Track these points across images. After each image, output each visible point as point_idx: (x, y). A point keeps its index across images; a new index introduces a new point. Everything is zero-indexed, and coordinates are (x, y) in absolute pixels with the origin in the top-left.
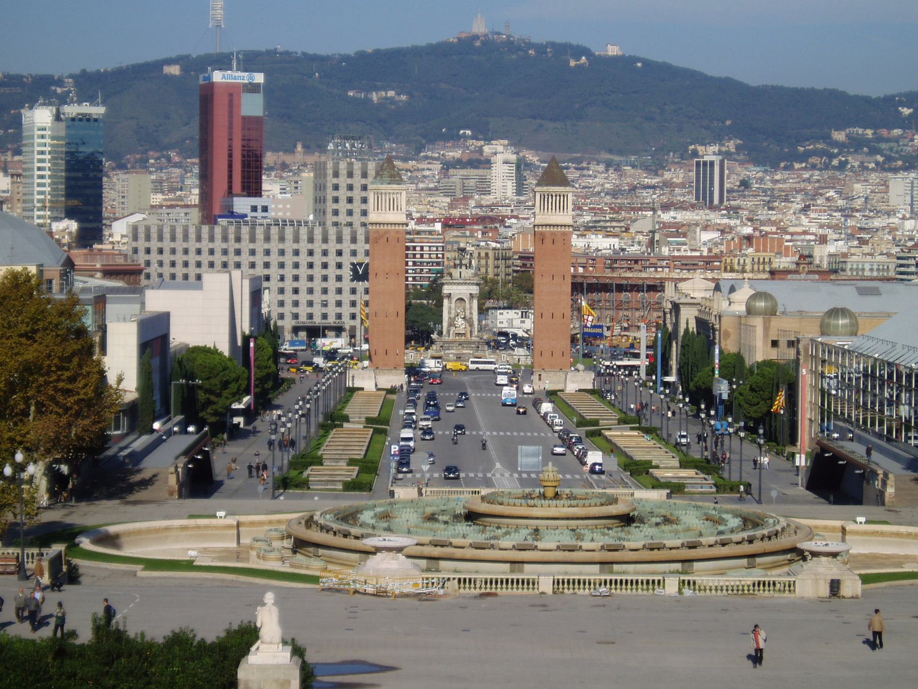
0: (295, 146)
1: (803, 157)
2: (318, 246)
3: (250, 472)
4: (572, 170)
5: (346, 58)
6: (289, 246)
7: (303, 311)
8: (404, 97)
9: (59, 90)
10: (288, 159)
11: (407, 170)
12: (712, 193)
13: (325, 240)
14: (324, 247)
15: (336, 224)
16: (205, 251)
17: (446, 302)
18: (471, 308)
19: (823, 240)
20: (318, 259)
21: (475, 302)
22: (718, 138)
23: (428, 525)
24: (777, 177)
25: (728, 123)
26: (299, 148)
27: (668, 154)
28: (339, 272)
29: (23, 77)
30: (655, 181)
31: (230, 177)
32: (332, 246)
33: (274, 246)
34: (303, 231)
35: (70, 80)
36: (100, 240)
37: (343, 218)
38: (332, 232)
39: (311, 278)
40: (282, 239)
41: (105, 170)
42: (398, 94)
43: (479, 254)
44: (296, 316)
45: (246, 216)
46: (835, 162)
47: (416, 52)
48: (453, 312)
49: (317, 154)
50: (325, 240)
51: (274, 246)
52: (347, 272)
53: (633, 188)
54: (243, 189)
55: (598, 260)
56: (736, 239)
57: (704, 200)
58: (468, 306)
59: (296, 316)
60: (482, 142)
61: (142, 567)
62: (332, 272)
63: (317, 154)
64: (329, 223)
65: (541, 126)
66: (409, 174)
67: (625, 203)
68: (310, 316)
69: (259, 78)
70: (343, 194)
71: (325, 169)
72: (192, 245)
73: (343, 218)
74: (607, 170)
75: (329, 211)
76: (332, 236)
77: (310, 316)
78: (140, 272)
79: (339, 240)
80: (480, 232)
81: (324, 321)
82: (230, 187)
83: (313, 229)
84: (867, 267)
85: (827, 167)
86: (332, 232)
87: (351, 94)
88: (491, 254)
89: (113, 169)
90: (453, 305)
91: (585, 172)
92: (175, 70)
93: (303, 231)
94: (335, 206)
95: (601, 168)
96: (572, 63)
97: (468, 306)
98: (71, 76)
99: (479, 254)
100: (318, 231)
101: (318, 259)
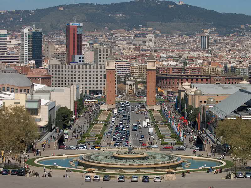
0: (94, 30)
1: (233, 33)
2: (95, 70)
4: (169, 37)
5: (108, 5)
9: (30, 14)
11: (125, 37)
12: (205, 46)
13: (97, 68)
14: (97, 70)
15: (100, 64)
16: (67, 71)
18: (133, 87)
19: (230, 62)
21: (134, 85)
22: (210, 28)
24: (225, 39)
25: (212, 23)
26: (95, 30)
28: (82, 76)
29: (20, 11)
30: (192, 40)
31: (74, 46)
32: (99, 70)
34: (92, 66)
36: (41, 66)
37: (102, 63)
38: (99, 66)
39: (94, 81)
41: (43, 37)
45: (77, 62)
46: (241, 34)
47: (127, 3)
48: (129, 88)
50: (97, 68)
51: (84, 70)
52: (103, 76)
53: (185, 43)
55: (170, 69)
56: (207, 63)
57: (203, 48)
59: (90, 88)
61: (47, 168)
62: (99, 76)
64: (98, 64)
65: (161, 24)
66: (125, 38)
67: (182, 46)
69: (81, 24)
70: (102, 57)
71: (97, 50)
73: (102, 63)
74: (179, 37)
75: (98, 61)
76: (99, 68)
77: (93, 88)
78: (50, 78)
79: (101, 68)
80: (140, 60)
83: (94, 66)
84: (241, 70)
85: (239, 36)
86: (99, 66)
88: (142, 67)
89: (45, 37)
91: (173, 37)
92: (62, 9)
93: (92, 66)
94: (100, 60)
95: (177, 36)
96: (170, 7)
97: (132, 86)
98: (33, 11)
100: (95, 66)
101: (95, 76)
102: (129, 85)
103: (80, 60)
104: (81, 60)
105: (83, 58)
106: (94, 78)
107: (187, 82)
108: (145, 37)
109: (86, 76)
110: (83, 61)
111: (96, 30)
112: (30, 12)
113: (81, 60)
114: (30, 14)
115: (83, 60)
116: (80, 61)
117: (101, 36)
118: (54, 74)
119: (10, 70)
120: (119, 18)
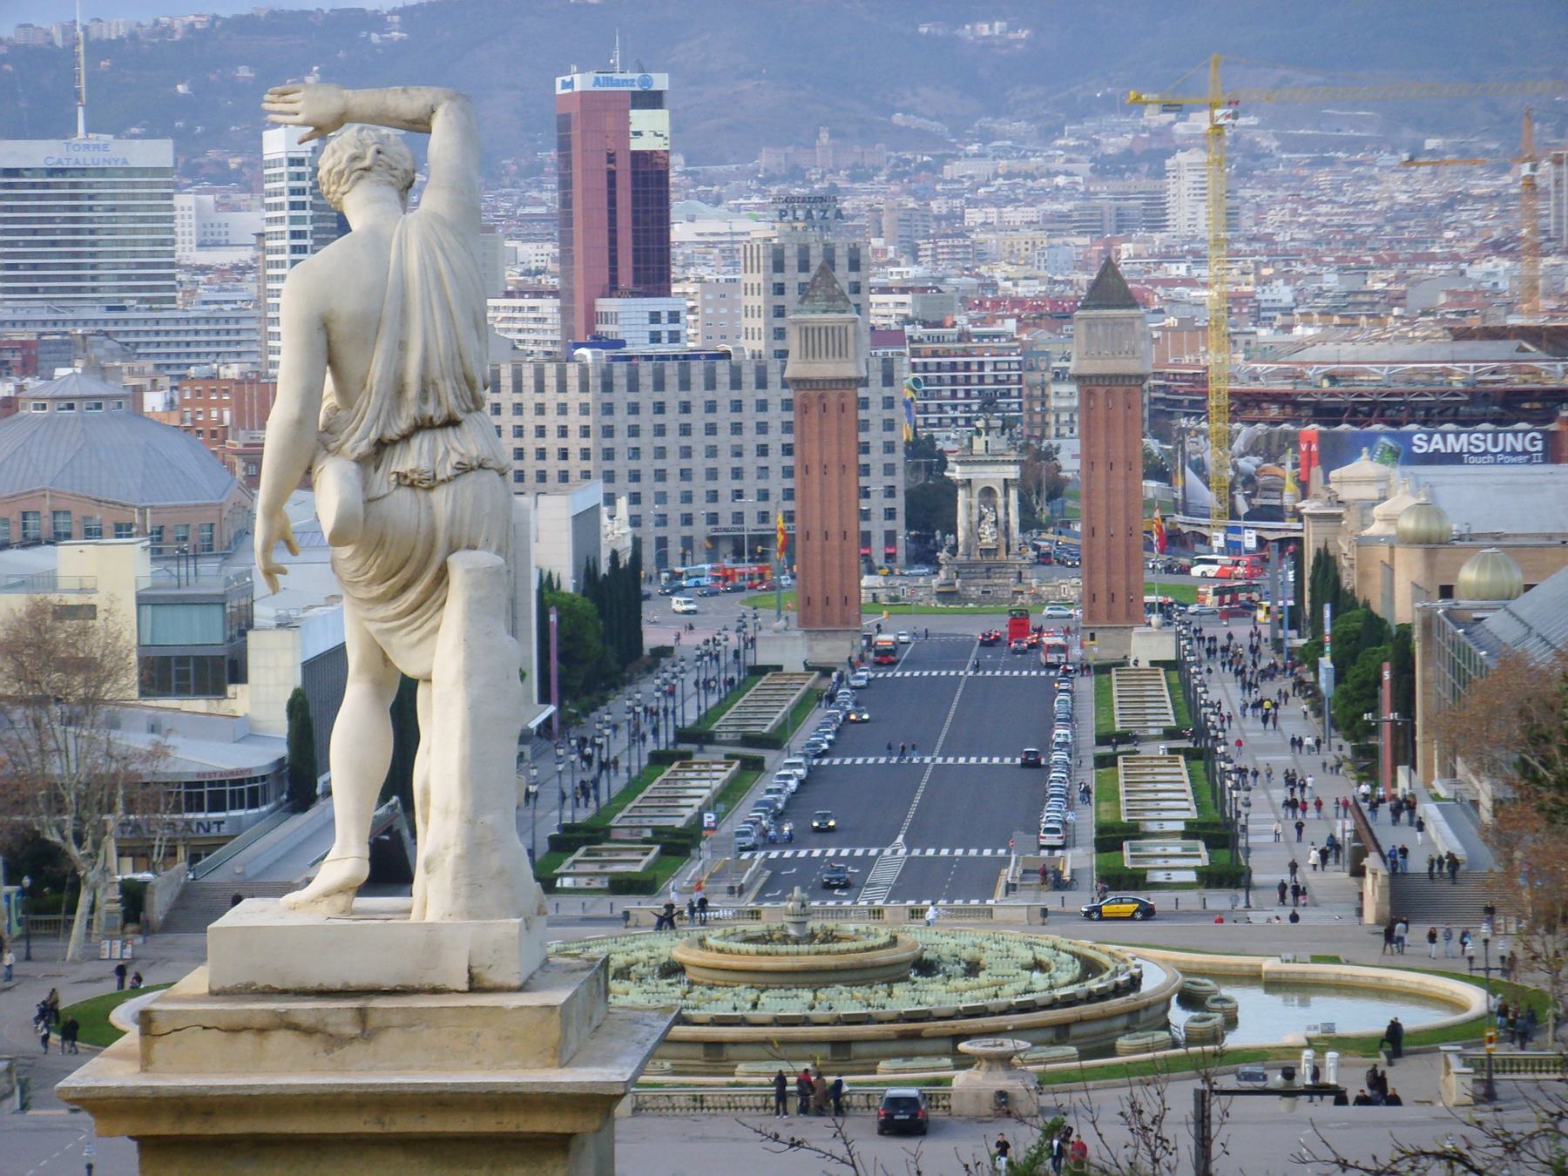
0: (817, 135)
3: (1283, 897)
6: (698, 395)
7: (725, 508)
8: (1023, 34)
9: (375, 37)
14: (735, 395)
17: (961, 494)
18: (1006, 506)
20: (698, 419)
23: (1219, 900)
26: (824, 137)
28: (685, 441)
33: (672, 396)
35: (396, 18)
40: (685, 384)
42: (1013, 28)
44: (713, 519)
49: (857, 149)
51: (672, 396)
54: (636, 281)
59: (713, 519)
68: (738, 517)
81: (763, 526)
82: (614, 279)
87: (924, 30)
90: (975, 501)
97: (1000, 501)
98: (394, 12)
102: (976, 492)
103: (656, 327)
104: (665, 327)
105: (674, 317)
106: (712, 452)
107: (1365, 456)
108: (1160, 174)
109: (685, 441)
110: (675, 337)
111: (833, 135)
112: (376, 21)
113: (665, 327)
114: (375, 37)
115: (656, 327)
116: (655, 338)
117: (860, 174)
118: (530, 452)
119: (77, 392)
120: (987, 44)
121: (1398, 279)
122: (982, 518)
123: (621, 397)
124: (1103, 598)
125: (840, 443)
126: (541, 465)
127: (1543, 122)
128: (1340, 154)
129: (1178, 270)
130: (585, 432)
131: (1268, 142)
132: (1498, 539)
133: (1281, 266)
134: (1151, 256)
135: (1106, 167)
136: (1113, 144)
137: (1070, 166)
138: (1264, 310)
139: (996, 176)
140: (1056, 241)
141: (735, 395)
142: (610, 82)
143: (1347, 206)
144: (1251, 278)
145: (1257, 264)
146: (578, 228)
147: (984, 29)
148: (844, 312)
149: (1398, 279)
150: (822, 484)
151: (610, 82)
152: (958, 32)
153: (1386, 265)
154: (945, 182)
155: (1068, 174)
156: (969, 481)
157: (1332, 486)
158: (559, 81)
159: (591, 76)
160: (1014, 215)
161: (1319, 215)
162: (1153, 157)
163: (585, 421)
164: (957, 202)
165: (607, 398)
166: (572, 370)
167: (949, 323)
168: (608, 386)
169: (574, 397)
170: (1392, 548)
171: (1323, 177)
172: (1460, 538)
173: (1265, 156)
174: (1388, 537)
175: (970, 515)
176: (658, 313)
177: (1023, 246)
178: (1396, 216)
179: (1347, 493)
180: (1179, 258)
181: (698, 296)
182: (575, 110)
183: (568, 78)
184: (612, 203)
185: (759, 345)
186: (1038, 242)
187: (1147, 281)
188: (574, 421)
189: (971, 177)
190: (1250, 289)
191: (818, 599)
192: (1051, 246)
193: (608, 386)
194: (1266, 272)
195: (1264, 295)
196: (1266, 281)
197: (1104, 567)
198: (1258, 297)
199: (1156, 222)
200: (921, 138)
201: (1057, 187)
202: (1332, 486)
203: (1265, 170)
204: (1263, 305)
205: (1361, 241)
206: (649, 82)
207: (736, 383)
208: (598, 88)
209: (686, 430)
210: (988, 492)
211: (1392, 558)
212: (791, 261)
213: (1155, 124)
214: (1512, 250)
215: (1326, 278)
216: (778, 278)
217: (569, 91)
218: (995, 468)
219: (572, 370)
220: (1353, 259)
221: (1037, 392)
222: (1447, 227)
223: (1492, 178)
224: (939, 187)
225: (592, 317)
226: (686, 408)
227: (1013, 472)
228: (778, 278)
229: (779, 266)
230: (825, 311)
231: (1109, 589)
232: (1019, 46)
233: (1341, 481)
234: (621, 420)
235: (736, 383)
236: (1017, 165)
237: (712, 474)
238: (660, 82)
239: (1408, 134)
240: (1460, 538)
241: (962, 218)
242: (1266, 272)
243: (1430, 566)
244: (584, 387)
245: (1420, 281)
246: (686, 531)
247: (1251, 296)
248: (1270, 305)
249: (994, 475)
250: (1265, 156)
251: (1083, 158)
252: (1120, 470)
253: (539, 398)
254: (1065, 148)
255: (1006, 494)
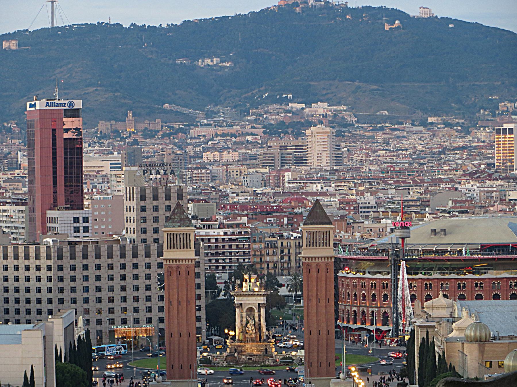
10: (119, 126)
14: (122, 261)
17: (237, 310)
18: (259, 317)
21: (263, 310)
26: (130, 115)
27: (479, 111)
43: (282, 243)
49: (147, 122)
58: (257, 314)
60: (303, 106)
62: (142, 282)
63: (147, 122)
72: (22, 262)
80: (286, 219)
82: (55, 200)
87: (178, 62)
90: (244, 314)
96: (387, 27)
97: (257, 314)
99: (282, 243)
102: (245, 310)
103: (77, 225)
104: (81, 225)
113: (81, 225)
115: (77, 225)
116: (77, 230)
117: (149, 134)
121: (425, 193)
122: (247, 322)
123: (67, 262)
124: (315, 365)
125: (187, 290)
126: (28, 295)
127: (485, 110)
128: (387, 125)
129: (317, 187)
130: (50, 279)
131: (351, 118)
132: (512, 339)
133: (368, 185)
134: (301, 179)
135: (273, 131)
136: (273, 119)
137: (253, 131)
138: (361, 208)
139: (217, 135)
140: (251, 170)
141: (122, 261)
142: (53, 104)
143: (394, 151)
144: (354, 191)
145: (355, 184)
146: (38, 175)
147: (208, 61)
148: (189, 226)
149: (425, 193)
150: (178, 310)
151: (53, 104)
152: (196, 63)
153: (416, 184)
154: (191, 138)
155: (252, 134)
156: (241, 304)
157: (425, 310)
158: (28, 104)
159: (44, 101)
160: (229, 156)
161: (379, 156)
162: (299, 127)
163: (49, 274)
164: (198, 149)
165: (60, 263)
166: (43, 249)
167: (214, 219)
168: (60, 257)
169: (44, 262)
170: (463, 344)
171: (379, 137)
172: (495, 339)
173: (350, 125)
174: (460, 338)
175: (241, 321)
176: (78, 218)
177: (235, 173)
178: (419, 156)
179: (435, 313)
180: (317, 181)
181: (90, 206)
182: (37, 118)
183: (33, 103)
184: (55, 163)
185: (134, 236)
186: (243, 171)
187: (303, 194)
188: (44, 273)
189: (204, 136)
190: (354, 197)
191: (177, 365)
192: (249, 174)
193: (60, 257)
194: (362, 188)
195: (361, 200)
196: (363, 193)
197: (316, 349)
198: (358, 201)
199: (301, 161)
200: (178, 116)
201: (248, 141)
202: (425, 310)
203: (350, 132)
204: (361, 205)
205: (402, 171)
206: (71, 104)
207: (123, 255)
208: (48, 108)
209: (98, 278)
210: (251, 310)
211: (463, 348)
212: (149, 195)
213: (294, 109)
214: (479, 177)
215: (390, 191)
216: (143, 203)
217: (33, 109)
218: (254, 298)
219: (43, 249)
220: (402, 182)
221: (258, 253)
222: (444, 164)
223: (462, 138)
224: (188, 141)
225: (45, 220)
226: (98, 267)
227: (262, 300)
228: (143, 203)
229: (143, 198)
230: (179, 226)
231: (318, 361)
232: (226, 70)
233: (432, 307)
234: (67, 273)
235: (123, 255)
236: (226, 130)
237: (86, 289)
238: (78, 104)
239: (419, 114)
240: (495, 339)
241: (202, 157)
242: (362, 188)
243: (482, 351)
244: (49, 257)
245: (436, 193)
246: (99, 327)
247: (355, 201)
248: (364, 205)
249: (253, 302)
250: (350, 125)
251: (259, 126)
252: (323, 303)
253: (27, 263)
254: (250, 121)
255: (259, 311)
